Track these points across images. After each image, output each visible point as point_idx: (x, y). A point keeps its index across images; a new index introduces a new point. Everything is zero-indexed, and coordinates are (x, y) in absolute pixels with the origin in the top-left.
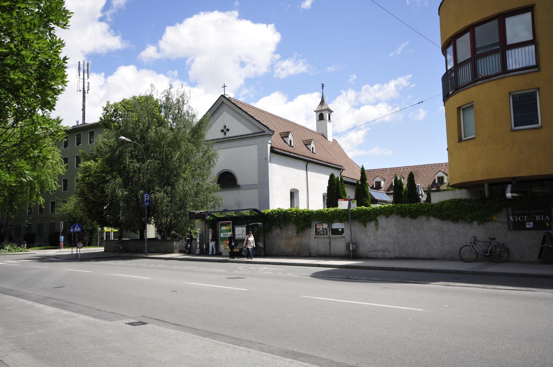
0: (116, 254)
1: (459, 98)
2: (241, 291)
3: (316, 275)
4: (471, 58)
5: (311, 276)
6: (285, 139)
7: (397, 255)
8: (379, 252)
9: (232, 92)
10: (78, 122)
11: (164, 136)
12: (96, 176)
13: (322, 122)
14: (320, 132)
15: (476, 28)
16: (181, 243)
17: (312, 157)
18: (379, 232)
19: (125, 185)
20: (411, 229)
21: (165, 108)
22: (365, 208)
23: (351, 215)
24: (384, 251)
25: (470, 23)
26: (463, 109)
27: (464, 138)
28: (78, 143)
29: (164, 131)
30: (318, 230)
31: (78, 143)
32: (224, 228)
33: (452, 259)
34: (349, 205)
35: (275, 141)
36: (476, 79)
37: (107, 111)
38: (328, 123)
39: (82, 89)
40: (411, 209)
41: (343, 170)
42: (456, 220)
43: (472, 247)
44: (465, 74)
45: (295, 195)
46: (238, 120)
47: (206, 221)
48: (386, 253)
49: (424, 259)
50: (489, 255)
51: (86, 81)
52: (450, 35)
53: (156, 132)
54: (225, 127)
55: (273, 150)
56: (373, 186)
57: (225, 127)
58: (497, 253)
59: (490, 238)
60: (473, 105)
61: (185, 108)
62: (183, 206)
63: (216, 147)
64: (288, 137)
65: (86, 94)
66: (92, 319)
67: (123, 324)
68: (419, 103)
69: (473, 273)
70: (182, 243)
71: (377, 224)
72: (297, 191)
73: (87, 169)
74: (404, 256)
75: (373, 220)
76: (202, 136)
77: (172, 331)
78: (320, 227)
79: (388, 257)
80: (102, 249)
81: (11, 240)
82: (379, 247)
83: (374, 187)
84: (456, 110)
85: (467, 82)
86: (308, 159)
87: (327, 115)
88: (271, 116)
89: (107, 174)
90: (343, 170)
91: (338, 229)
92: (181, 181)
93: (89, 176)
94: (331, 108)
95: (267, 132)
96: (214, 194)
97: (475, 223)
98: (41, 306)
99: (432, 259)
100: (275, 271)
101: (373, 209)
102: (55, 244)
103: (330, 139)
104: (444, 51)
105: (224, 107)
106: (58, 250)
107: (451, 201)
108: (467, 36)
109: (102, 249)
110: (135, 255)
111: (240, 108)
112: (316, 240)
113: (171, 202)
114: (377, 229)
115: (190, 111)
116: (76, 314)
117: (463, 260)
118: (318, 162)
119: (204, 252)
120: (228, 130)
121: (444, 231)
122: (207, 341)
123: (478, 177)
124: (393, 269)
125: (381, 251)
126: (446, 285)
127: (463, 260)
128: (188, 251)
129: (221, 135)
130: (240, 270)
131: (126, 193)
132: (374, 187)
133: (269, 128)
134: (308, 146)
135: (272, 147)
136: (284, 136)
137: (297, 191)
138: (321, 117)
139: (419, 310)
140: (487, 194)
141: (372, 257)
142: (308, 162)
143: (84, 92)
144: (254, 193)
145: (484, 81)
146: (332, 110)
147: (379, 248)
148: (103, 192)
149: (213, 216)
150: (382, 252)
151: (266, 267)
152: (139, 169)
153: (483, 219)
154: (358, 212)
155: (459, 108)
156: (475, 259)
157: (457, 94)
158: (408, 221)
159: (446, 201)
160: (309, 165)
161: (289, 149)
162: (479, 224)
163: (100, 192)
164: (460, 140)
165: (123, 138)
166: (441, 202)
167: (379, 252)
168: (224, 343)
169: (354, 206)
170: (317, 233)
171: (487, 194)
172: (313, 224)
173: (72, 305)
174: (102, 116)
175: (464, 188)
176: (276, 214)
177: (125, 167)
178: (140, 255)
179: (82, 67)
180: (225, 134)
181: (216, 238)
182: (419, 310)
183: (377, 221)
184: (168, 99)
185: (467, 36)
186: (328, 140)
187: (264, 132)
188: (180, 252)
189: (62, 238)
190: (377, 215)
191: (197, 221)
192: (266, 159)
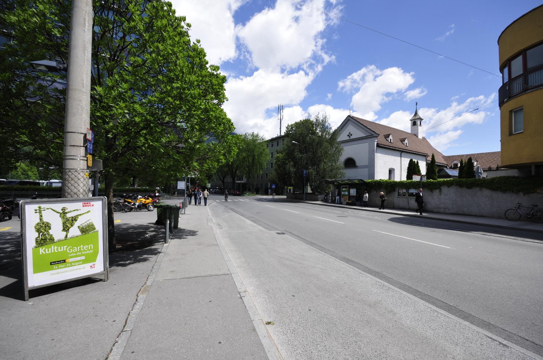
0: (291, 200)
1: (512, 104)
2: (341, 224)
3: (392, 220)
4: (522, 74)
5: (388, 220)
6: (387, 138)
7: (454, 211)
8: (442, 209)
9: (373, 112)
10: (278, 135)
11: (314, 140)
12: (281, 161)
13: (415, 126)
14: (413, 133)
15: (527, 52)
16: (322, 196)
17: (405, 148)
18: (442, 196)
19: (294, 166)
20: (467, 196)
21: (315, 125)
22: (432, 180)
23: (422, 185)
24: (445, 209)
25: (522, 48)
26: (515, 112)
27: (515, 132)
28: (278, 145)
29: (314, 137)
30: (400, 193)
31: (278, 145)
32: (344, 189)
33: (499, 218)
34: (421, 179)
35: (381, 140)
36: (526, 90)
37: (288, 129)
38: (419, 127)
39: (280, 118)
40: (467, 182)
41: (428, 156)
42: (504, 191)
43: (517, 210)
44: (517, 86)
45: (392, 171)
46: (358, 129)
47: (335, 185)
48: (447, 210)
49: (475, 216)
50: (530, 218)
51: (282, 114)
52: (506, 59)
53: (310, 138)
54: (350, 133)
55: (378, 146)
56: (452, 166)
57: (350, 133)
58: (539, 216)
59: (533, 205)
60: (522, 109)
61: (326, 124)
62: (324, 177)
63: (342, 145)
64: (389, 137)
65: (282, 121)
66: (263, 229)
67: (274, 233)
68: (477, 109)
69: (512, 229)
70: (323, 196)
71: (440, 191)
72: (394, 169)
73: (278, 157)
74: (460, 213)
75: (438, 188)
76: (335, 139)
77: (294, 239)
78: (401, 191)
79: (448, 213)
80: (285, 197)
81: (250, 190)
82: (442, 206)
83: (453, 167)
84: (508, 113)
85: (520, 91)
86: (402, 150)
87: (419, 122)
88: (378, 125)
89: (286, 160)
90: (428, 156)
91: (413, 193)
92: (323, 163)
93: (279, 161)
94: (422, 117)
95: (375, 135)
96: (342, 171)
97: (521, 194)
98: (247, 220)
99: (482, 216)
100: (368, 215)
101: (438, 181)
102: (267, 194)
103: (420, 137)
104: (502, 70)
105: (350, 122)
106: (268, 196)
107: (501, 178)
108: (520, 58)
109: (285, 197)
110: (300, 201)
111: (359, 122)
112: (398, 199)
113: (317, 174)
114: (440, 194)
115: (329, 126)
116: (258, 226)
117: (507, 219)
118: (410, 151)
119: (333, 202)
120: (351, 135)
121: (493, 198)
122: (304, 246)
123: (524, 160)
124: (448, 220)
125: (443, 208)
126: (483, 235)
127: (508, 219)
128: (325, 200)
129: (348, 138)
130: (349, 213)
131: (295, 170)
132: (453, 167)
133: (376, 133)
134: (403, 142)
135: (377, 144)
136: (387, 136)
137: (394, 169)
138: (414, 124)
139: (447, 247)
140: (533, 173)
141: (436, 211)
142: (402, 152)
143: (281, 120)
144: (366, 170)
145: (533, 90)
146: (423, 118)
147: (441, 206)
148: (284, 169)
149: (338, 182)
150: (443, 209)
151: (364, 212)
152: (302, 157)
153: (527, 191)
154: (427, 183)
155: (511, 112)
156: (519, 219)
157: (513, 100)
158: (465, 190)
159: (497, 177)
160: (403, 154)
161: (390, 144)
162: (524, 195)
163: (283, 169)
164: (511, 134)
165: (294, 142)
166: (492, 178)
167: (442, 209)
168: (315, 249)
169: (425, 179)
170: (399, 195)
171: (533, 173)
172: (397, 189)
173: (259, 221)
174: (285, 131)
175: (516, 169)
176: (373, 182)
177: (295, 157)
178: (301, 201)
179: (280, 107)
180: (350, 137)
181: (339, 194)
182: (447, 247)
183: (441, 189)
184: (317, 120)
185: (520, 58)
186: (419, 137)
187: (373, 135)
188: (322, 201)
189: (270, 191)
190: (441, 186)
191: (330, 185)
192: (374, 151)
